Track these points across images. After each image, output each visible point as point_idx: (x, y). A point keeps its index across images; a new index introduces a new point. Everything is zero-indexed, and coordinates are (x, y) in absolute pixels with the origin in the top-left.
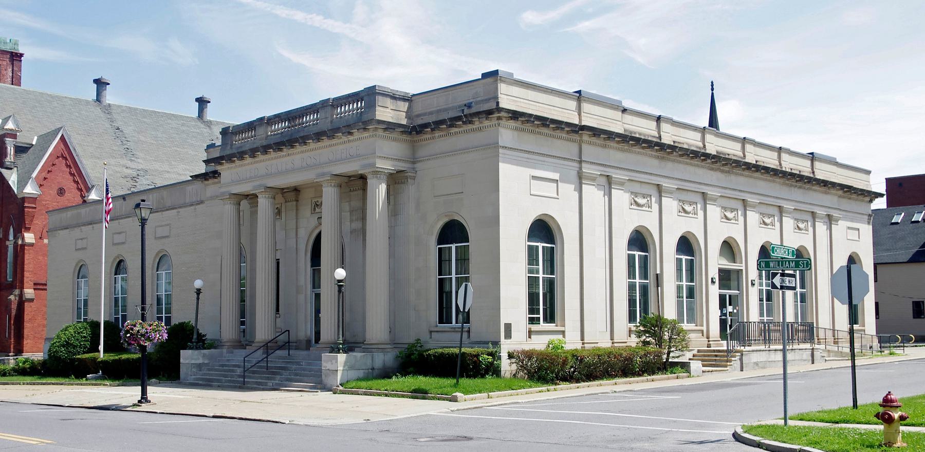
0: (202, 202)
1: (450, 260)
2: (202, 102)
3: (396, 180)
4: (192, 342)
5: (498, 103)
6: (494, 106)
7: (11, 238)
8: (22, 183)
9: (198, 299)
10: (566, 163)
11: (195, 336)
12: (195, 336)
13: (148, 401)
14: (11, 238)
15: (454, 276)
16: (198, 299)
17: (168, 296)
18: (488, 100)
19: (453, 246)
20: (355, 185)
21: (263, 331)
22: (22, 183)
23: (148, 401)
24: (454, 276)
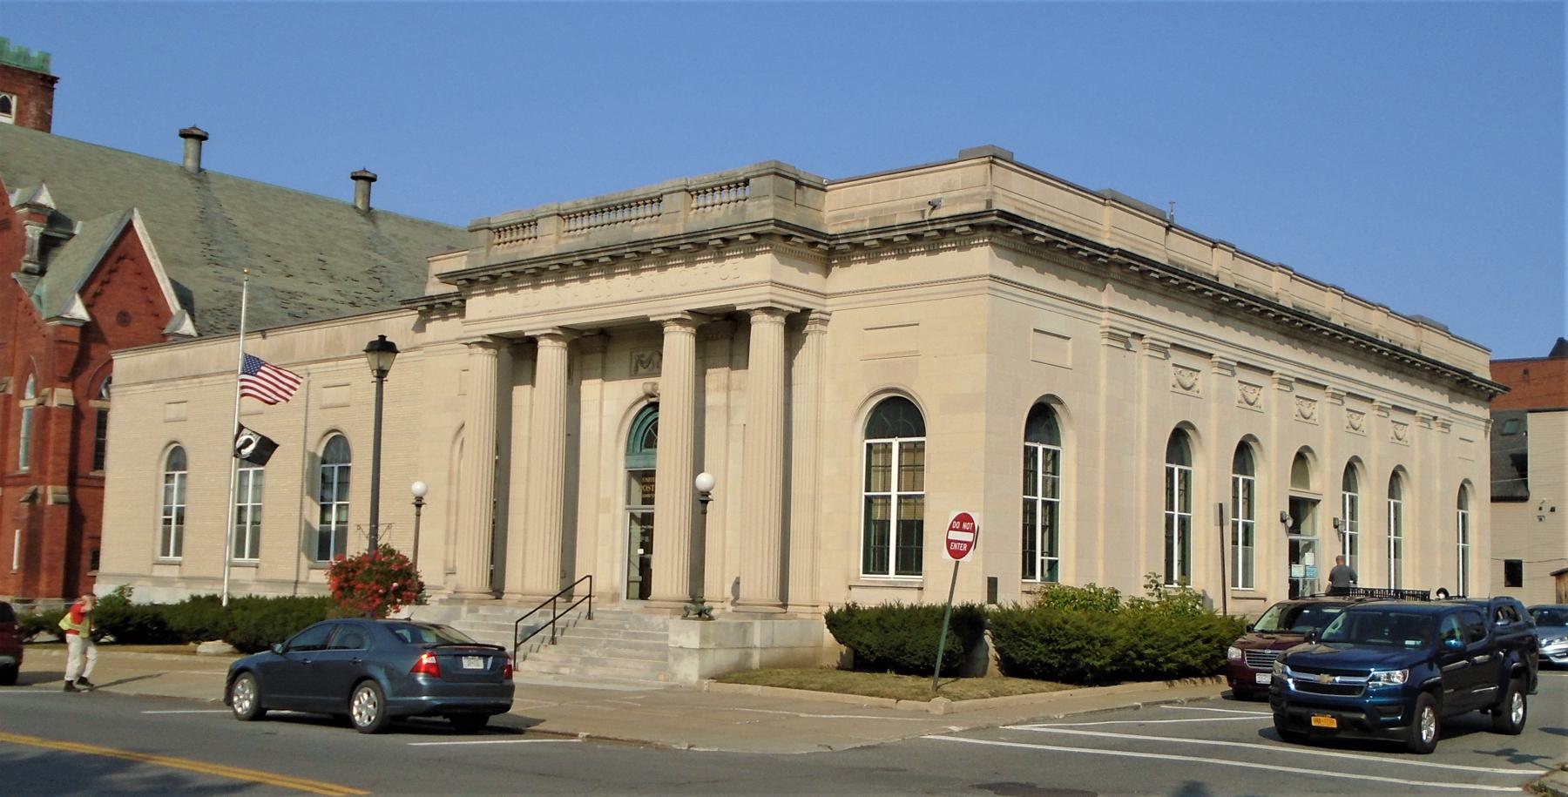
3: (796, 325)
15: (894, 493)
16: (418, 515)
19: (895, 443)
24: (894, 493)
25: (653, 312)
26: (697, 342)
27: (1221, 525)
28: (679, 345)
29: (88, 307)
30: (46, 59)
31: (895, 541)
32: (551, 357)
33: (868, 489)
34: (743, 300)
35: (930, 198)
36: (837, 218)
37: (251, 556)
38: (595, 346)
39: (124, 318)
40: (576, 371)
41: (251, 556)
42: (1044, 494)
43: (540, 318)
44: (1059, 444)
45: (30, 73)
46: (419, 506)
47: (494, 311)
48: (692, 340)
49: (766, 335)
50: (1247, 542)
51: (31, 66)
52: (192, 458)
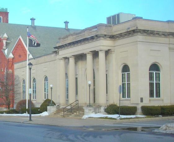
0: (56, 60)
1: (125, 78)
2: (66, 23)
3: (107, 52)
4: (50, 104)
5: (137, 27)
6: (136, 28)
7: (5, 71)
8: (8, 53)
9: (52, 90)
10: (162, 44)
11: (51, 102)
12: (51, 102)
13: (32, 121)
14: (5, 71)
15: (126, 83)
16: (52, 90)
17: (25, 91)
18: (134, 26)
19: (126, 73)
20: (95, 54)
21: (72, 100)
22: (8, 53)
23: (32, 121)
24: (126, 83)
25: (85, 52)
26: (93, 57)
27: (94, 89)
28: (89, 57)
29: (13, 55)
30: (7, 9)
31: (125, 90)
32: (72, 61)
33: (123, 82)
34: (68, 56)
35: (65, 44)
36: (115, 32)
37: (157, 96)
38: (80, 57)
39: (20, 56)
40: (76, 62)
41: (157, 96)
42: (127, 82)
43: (105, 47)
44: (159, 71)
45: (4, 12)
46: (51, 89)
47: (64, 53)
48: (74, 60)
49: (102, 55)
50: (25, 93)
51: (4, 11)
52: (48, 78)
